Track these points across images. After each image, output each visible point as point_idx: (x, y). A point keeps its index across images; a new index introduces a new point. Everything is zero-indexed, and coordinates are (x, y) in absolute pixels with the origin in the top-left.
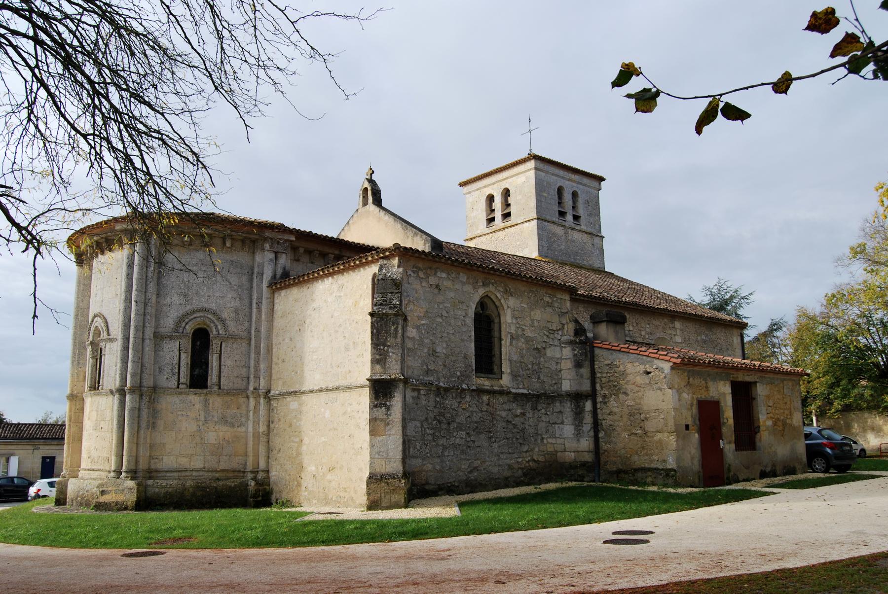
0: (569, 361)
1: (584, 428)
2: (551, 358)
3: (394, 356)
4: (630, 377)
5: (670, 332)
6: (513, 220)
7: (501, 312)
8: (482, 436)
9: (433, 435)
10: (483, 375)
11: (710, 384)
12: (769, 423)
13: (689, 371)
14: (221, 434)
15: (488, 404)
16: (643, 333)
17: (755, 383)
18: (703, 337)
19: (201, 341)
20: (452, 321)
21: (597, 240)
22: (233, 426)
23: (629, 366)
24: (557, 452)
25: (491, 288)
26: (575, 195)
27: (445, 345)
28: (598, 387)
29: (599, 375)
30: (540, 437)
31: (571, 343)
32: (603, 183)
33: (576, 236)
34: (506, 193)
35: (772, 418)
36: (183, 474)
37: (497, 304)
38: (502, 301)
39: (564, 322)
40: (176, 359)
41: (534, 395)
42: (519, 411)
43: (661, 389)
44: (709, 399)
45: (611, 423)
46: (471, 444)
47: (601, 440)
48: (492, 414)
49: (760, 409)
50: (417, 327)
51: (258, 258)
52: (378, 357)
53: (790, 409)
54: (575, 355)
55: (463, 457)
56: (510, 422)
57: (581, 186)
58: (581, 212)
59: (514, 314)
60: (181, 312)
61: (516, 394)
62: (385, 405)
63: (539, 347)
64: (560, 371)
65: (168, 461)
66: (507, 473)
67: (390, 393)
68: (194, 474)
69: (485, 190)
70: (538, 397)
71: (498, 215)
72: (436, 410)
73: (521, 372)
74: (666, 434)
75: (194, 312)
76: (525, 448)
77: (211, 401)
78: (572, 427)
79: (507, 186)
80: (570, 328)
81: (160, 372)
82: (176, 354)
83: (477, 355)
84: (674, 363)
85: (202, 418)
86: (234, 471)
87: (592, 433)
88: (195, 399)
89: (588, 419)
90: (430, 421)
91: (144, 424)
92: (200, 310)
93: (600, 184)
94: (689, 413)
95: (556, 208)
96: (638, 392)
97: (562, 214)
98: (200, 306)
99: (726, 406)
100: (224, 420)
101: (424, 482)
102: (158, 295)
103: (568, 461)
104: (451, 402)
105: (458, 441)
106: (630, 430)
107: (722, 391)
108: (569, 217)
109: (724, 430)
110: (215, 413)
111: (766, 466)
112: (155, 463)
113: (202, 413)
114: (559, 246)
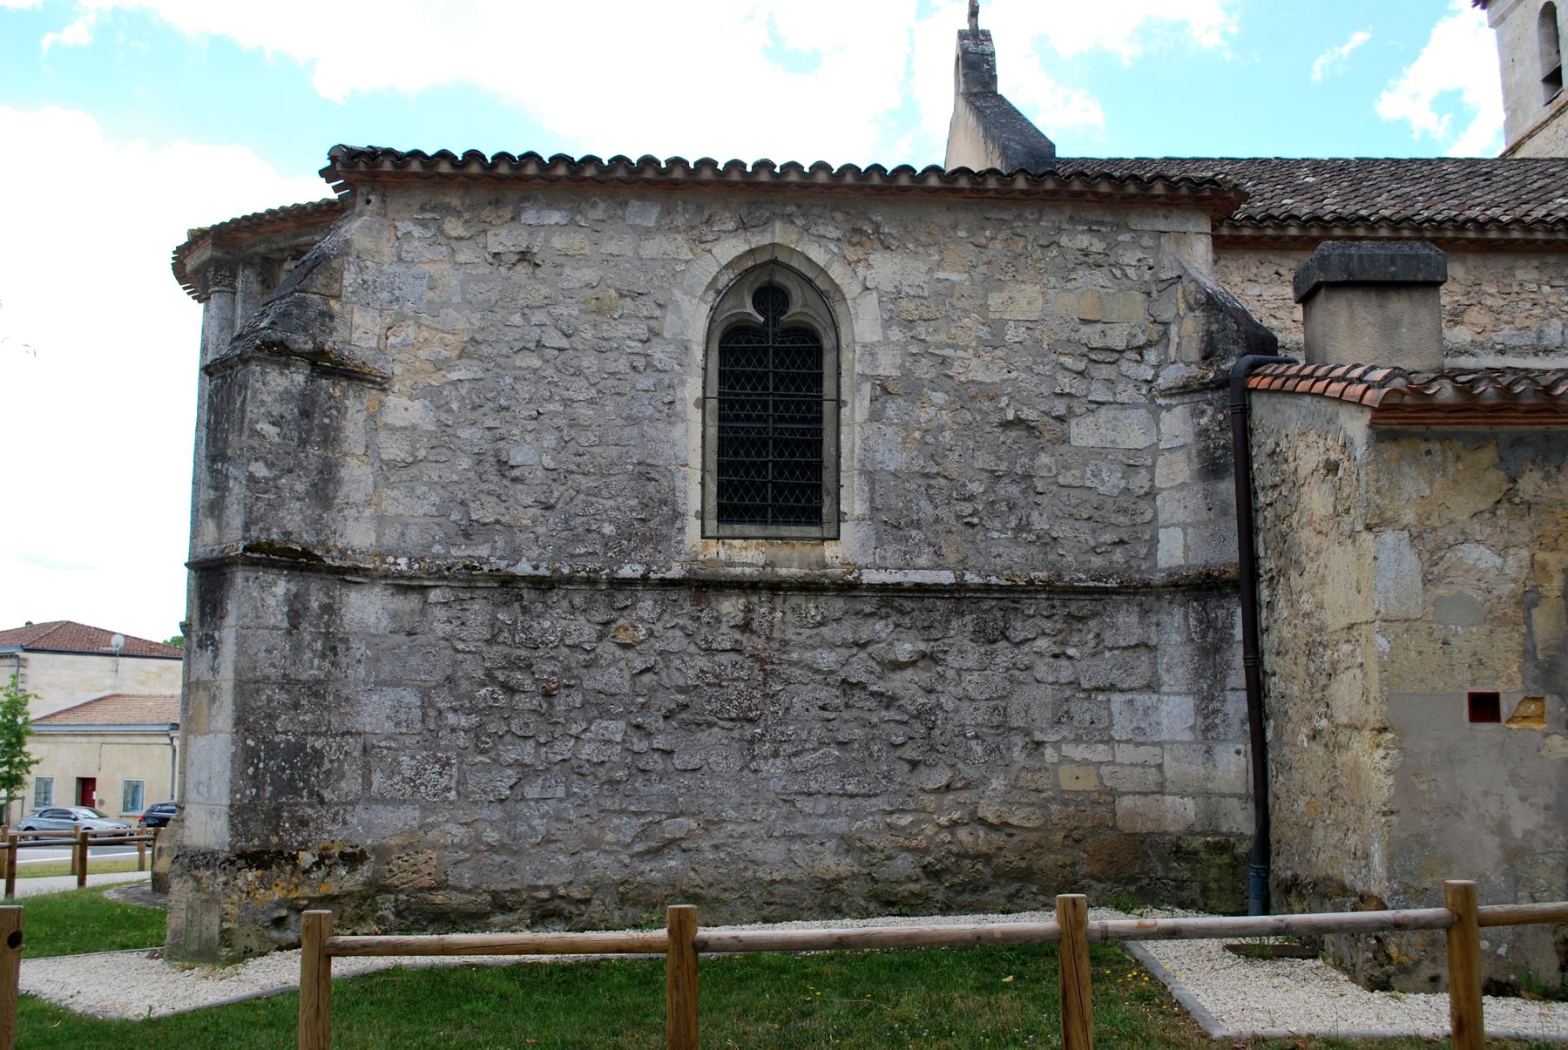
0: (1180, 456)
2: (1100, 452)
7: (839, 309)
9: (476, 732)
10: (751, 530)
15: (745, 627)
20: (589, 362)
24: (1114, 794)
27: (550, 440)
30: (1019, 740)
31: (1183, 389)
38: (837, 272)
39: (1165, 317)
41: (988, 588)
42: (905, 649)
48: (763, 661)
50: (433, 395)
54: (1203, 433)
56: (861, 686)
61: (883, 587)
63: (1029, 414)
66: (832, 863)
70: (1012, 594)
72: (496, 651)
78: (1189, 703)
80: (1188, 331)
90: (465, 686)
101: (427, 881)
104: (563, 623)
105: (587, 751)
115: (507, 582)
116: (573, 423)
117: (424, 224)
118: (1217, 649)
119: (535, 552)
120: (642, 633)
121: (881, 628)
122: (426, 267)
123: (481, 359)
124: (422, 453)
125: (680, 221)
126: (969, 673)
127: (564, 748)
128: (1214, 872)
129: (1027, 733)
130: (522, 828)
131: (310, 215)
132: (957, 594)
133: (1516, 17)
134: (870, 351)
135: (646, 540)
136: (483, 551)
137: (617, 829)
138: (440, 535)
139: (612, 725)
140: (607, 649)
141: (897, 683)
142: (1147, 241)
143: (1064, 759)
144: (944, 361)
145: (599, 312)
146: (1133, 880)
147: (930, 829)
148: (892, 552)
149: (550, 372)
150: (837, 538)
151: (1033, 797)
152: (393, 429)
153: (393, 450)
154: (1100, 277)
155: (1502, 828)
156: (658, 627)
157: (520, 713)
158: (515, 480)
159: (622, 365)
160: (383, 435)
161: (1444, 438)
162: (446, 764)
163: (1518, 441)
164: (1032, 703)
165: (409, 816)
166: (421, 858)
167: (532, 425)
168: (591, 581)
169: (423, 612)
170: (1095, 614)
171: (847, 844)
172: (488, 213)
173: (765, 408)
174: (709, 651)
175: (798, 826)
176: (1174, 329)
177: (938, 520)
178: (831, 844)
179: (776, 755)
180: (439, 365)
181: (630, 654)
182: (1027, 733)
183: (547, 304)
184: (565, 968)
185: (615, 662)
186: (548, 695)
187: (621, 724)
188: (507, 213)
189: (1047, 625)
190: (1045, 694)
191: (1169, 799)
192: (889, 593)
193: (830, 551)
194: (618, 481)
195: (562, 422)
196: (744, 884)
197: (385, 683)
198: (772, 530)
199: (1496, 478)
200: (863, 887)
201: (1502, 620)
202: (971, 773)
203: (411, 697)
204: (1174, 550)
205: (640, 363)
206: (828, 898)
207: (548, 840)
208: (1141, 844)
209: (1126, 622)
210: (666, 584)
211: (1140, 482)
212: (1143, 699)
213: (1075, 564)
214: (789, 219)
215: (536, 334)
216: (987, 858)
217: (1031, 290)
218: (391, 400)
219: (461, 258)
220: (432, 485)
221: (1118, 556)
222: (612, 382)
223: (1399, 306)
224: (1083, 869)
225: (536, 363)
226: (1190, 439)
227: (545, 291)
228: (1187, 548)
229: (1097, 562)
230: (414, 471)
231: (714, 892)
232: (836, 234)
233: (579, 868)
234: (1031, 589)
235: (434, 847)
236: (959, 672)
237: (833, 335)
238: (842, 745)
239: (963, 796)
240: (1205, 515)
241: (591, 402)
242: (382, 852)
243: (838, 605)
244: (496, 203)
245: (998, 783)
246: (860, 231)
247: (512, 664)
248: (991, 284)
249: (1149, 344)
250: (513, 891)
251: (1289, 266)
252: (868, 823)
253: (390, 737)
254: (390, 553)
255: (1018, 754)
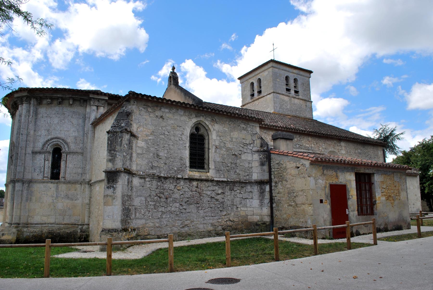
0: (257, 162)
1: (265, 202)
2: (245, 160)
3: (120, 157)
4: (289, 171)
5: (338, 148)
6: (263, 94)
7: (209, 133)
8: (192, 206)
9: (155, 205)
10: (195, 170)
11: (339, 174)
12: (384, 198)
13: (324, 166)
14: (65, 204)
15: (197, 187)
16: (320, 148)
17: (373, 174)
18: (359, 151)
19: (57, 154)
20: (172, 138)
21: (308, 103)
22: (72, 200)
23: (288, 163)
24: (247, 215)
25: (202, 119)
26: (295, 80)
27: (166, 151)
28: (273, 177)
29: (273, 170)
30: (235, 207)
31: (258, 151)
32: (312, 74)
33: (296, 101)
34: (259, 80)
35: (385, 195)
36: (44, 225)
37: (207, 128)
38: (210, 126)
39: (254, 139)
40: (43, 164)
41: (231, 182)
42: (220, 192)
43: (304, 177)
44: (338, 183)
45: (279, 198)
46: (184, 211)
47: (274, 209)
48: (200, 193)
49: (376, 190)
50: (146, 141)
51: (88, 110)
52: (110, 158)
53: (398, 190)
54: (261, 158)
55: (177, 218)
56: (214, 198)
57: (299, 76)
58: (300, 89)
59: (217, 134)
60: (46, 139)
61: (217, 181)
62: (113, 187)
63: (236, 153)
64: (252, 168)
65: (37, 219)
66: (210, 228)
67: (116, 179)
68: (50, 225)
69: (250, 80)
70: (234, 183)
71: (256, 93)
72: (158, 190)
73: (222, 168)
74: (307, 205)
75: (52, 139)
76: (225, 213)
77: (60, 186)
78: (258, 201)
79: (259, 77)
80: (258, 142)
81: (35, 171)
82: (44, 163)
83: (191, 158)
84: (311, 161)
85: (55, 196)
86: (72, 224)
87: (269, 205)
88: (52, 186)
89: (267, 196)
90: (152, 197)
91: (24, 199)
92: (56, 138)
93: (310, 74)
94: (323, 192)
95: (285, 87)
96: (293, 179)
97: (288, 90)
98: (55, 136)
99: (351, 187)
100: (67, 197)
101: (146, 234)
102: (35, 131)
103: (255, 221)
104: (169, 185)
105: (173, 209)
106: (288, 203)
107: (349, 179)
108: (292, 92)
109: (350, 203)
110: (62, 193)
111: (380, 225)
112: (30, 219)
113: (55, 192)
114: (286, 106)
115: (160, 177)
116: (170, 149)
117: (144, 108)
118: (263, 192)
119: (164, 172)
120: (181, 188)
121: (217, 188)
122: (145, 117)
123: (154, 135)
124: (144, 152)
125: (187, 114)
126: (229, 196)
127: (169, 208)
128: (263, 227)
129: (236, 206)
130: (162, 223)
131: (59, 91)
132: (227, 183)
133: (245, 83)
134: (215, 140)
135: (181, 171)
136: (155, 171)
137: (178, 223)
138: (148, 168)
139: (177, 204)
140: (176, 190)
141: (219, 197)
142: (251, 127)
143: (241, 210)
144: (225, 143)
145: (174, 129)
146: (250, 229)
147: (223, 222)
148: (218, 175)
149: (166, 139)
150: (209, 172)
151: (237, 216)
152: (139, 147)
153: (139, 151)
154: (245, 132)
155: (323, 217)
156: (184, 187)
157: (162, 202)
158: (160, 158)
159: (177, 139)
160: (137, 148)
161: (317, 165)
162: (149, 211)
163: (324, 166)
164: (237, 201)
165: (143, 221)
166: (145, 229)
167: (163, 148)
168: (174, 178)
169: (144, 183)
170: (245, 186)
171: (212, 225)
172: (155, 108)
173: (196, 148)
174: (192, 191)
175: (205, 222)
176: (255, 142)
177: (224, 170)
178: (210, 225)
179: (202, 209)
180: (147, 136)
181: (179, 191)
182: (236, 206)
183: (166, 126)
184: (251, 239)
185: (177, 193)
186: (167, 199)
187: (178, 204)
188: (159, 109)
189: (239, 188)
190: (238, 199)
191: (255, 216)
192: (218, 182)
193: (208, 174)
194: (177, 160)
195: (168, 148)
196: (197, 232)
197: (139, 196)
198: (198, 170)
199: (322, 170)
200: (214, 232)
201: (323, 190)
202: (229, 212)
203: (143, 199)
204: (255, 177)
205: (180, 139)
206: (209, 234)
207: (167, 225)
208: (251, 223)
209: (249, 188)
210: (185, 179)
211: (250, 165)
212: (251, 200)
213: (242, 178)
214: (203, 116)
215: (163, 132)
216: (231, 226)
217: (237, 133)
218: (139, 141)
219: (151, 116)
220: (146, 158)
221: (248, 177)
222: (176, 142)
223: (288, 142)
224: (243, 228)
225: (164, 137)
226: (258, 159)
227: (165, 124)
228: (258, 176)
229: (245, 178)
230: (143, 155)
231: (193, 234)
232: (210, 120)
233: (172, 230)
234: (237, 182)
235: (147, 227)
236: (227, 195)
237: (208, 137)
238: (211, 208)
239: (228, 216)
240: (261, 171)
241: (173, 145)
242: (138, 228)
243: (210, 184)
244: (157, 106)
245: (232, 214)
246: (213, 120)
247: (160, 193)
248: (231, 131)
249: (252, 143)
250: (161, 235)
251: (272, 133)
252: (215, 221)
253: (139, 206)
254: (139, 171)
255: (235, 209)
